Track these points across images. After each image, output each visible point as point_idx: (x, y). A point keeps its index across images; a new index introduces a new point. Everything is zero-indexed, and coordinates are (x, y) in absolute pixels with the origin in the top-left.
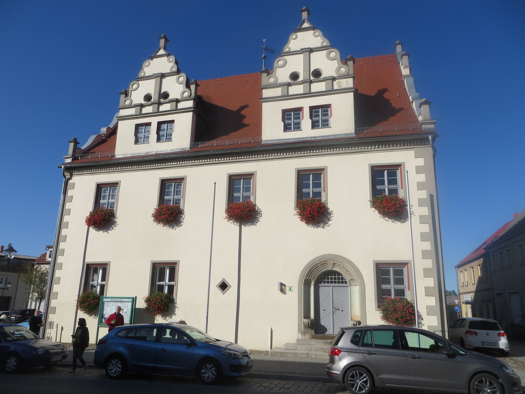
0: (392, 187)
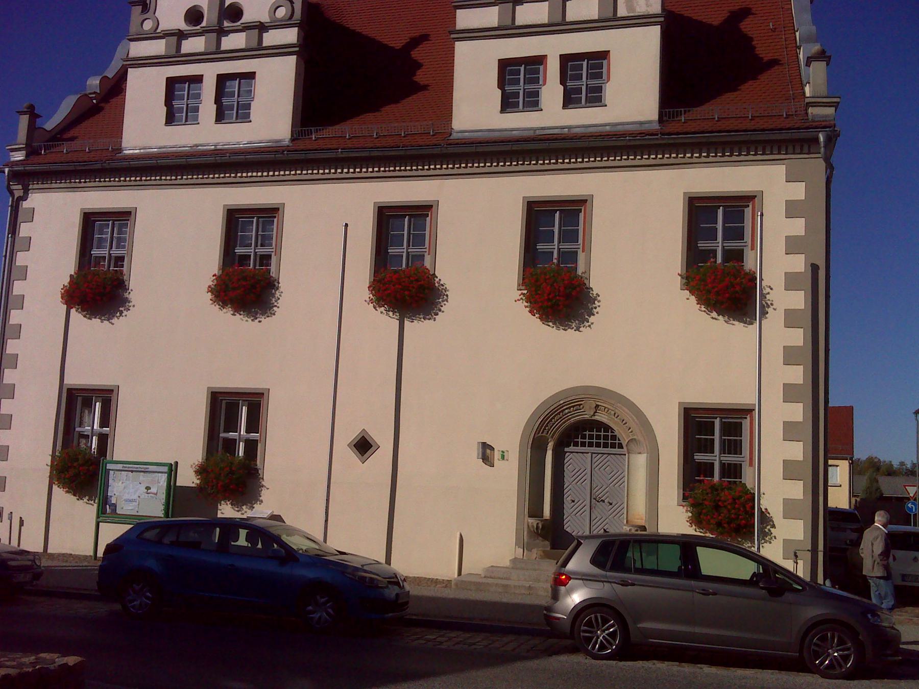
0: (733, 245)
